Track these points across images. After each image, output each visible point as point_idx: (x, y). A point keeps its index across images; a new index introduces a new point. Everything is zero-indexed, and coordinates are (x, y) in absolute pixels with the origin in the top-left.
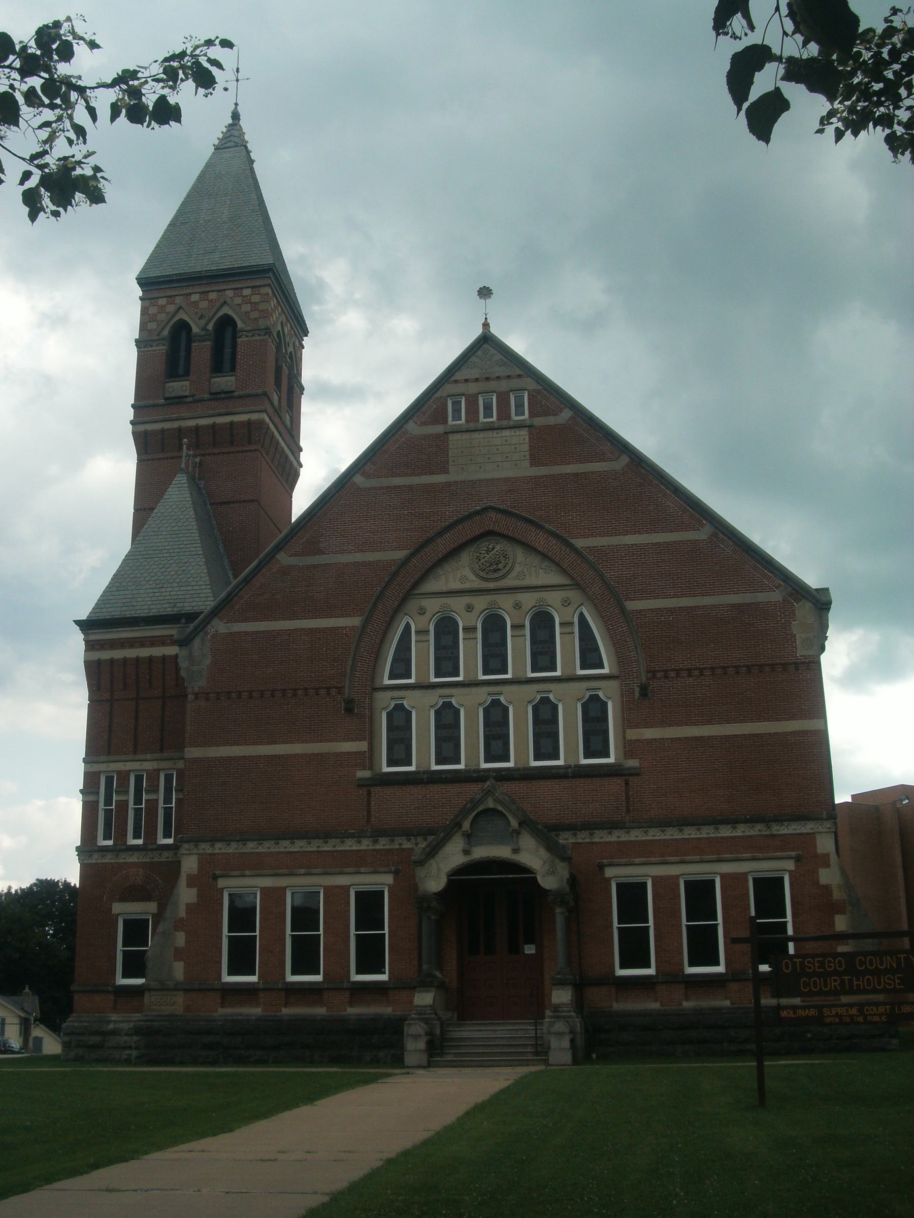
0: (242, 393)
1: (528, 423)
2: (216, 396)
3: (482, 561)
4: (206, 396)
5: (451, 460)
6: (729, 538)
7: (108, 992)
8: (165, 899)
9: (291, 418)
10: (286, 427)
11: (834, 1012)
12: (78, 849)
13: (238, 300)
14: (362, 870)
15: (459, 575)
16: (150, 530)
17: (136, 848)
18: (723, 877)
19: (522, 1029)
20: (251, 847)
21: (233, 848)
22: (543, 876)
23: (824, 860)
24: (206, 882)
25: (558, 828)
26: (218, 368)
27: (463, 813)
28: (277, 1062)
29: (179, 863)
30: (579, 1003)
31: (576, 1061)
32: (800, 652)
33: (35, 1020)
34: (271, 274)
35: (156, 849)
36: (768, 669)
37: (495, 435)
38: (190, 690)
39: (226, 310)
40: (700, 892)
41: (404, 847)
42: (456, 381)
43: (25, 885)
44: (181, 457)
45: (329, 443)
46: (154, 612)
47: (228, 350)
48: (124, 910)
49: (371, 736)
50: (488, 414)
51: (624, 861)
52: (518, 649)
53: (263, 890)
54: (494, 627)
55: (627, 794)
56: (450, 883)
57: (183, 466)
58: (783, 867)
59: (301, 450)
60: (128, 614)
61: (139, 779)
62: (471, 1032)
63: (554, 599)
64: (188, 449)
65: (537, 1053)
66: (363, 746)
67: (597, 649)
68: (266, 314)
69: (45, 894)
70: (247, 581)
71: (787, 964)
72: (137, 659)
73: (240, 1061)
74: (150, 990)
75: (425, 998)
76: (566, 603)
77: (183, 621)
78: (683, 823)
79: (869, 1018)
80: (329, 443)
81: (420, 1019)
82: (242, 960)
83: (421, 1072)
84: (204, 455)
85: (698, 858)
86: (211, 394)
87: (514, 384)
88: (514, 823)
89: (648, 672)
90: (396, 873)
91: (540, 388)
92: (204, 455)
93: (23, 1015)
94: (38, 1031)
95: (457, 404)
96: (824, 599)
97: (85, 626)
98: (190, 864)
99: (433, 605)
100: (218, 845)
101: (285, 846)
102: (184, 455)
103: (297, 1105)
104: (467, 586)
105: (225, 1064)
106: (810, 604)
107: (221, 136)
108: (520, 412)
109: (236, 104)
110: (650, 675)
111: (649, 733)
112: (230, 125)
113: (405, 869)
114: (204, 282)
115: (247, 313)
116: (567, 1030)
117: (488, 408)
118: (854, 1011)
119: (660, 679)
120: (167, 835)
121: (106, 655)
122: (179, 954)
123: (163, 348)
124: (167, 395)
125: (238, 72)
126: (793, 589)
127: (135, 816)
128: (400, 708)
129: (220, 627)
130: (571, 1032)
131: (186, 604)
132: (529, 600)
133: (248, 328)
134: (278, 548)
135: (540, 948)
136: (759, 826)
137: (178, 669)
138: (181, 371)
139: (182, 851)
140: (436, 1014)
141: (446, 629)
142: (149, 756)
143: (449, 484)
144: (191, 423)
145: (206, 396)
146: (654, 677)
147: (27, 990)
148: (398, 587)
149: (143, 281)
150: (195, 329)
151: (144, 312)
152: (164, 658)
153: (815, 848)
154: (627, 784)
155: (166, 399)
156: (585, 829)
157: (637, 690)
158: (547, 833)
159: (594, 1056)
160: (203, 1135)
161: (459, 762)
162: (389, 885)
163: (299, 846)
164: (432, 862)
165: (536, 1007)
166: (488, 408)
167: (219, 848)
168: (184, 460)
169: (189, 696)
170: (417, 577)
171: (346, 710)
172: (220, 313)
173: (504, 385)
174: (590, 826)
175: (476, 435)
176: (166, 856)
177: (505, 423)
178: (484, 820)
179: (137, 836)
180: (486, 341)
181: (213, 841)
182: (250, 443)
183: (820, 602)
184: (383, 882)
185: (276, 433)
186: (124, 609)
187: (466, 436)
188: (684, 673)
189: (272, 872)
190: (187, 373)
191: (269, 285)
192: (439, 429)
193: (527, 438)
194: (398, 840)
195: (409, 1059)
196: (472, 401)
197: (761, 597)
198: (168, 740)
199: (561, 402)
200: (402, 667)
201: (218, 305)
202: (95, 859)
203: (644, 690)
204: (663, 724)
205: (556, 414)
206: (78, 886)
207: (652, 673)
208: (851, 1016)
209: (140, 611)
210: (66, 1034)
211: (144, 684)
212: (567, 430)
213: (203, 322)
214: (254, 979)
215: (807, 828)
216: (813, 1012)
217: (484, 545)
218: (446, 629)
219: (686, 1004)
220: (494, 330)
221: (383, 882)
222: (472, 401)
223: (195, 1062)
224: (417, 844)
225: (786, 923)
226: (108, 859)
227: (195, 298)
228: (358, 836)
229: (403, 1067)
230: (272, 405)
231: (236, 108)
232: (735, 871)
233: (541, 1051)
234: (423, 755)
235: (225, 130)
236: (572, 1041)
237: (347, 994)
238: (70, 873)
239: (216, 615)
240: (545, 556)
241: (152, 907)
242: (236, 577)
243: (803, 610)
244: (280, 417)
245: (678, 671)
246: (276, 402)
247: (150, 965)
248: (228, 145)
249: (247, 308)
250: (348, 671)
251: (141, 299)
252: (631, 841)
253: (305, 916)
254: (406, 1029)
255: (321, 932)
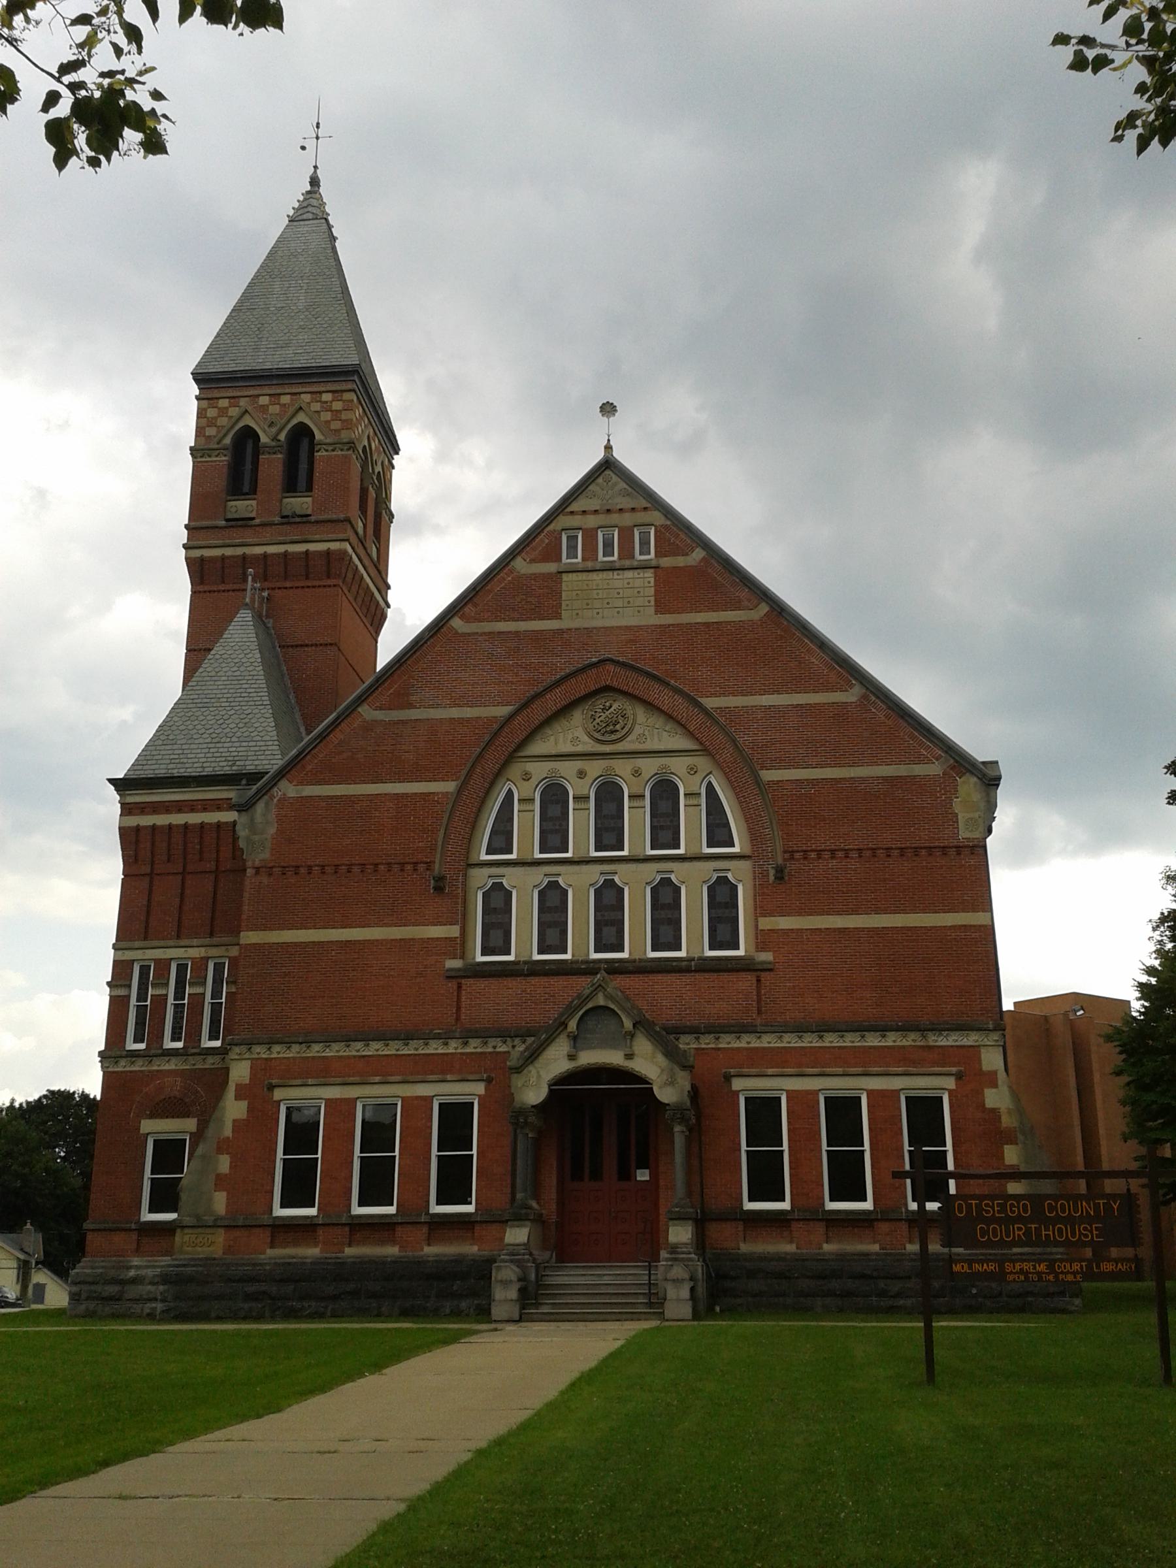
0: (321, 517)
1: (654, 563)
2: (290, 520)
3: (598, 720)
4: (277, 519)
5: (564, 604)
6: (882, 701)
7: (131, 1230)
8: (206, 1112)
9: (378, 550)
10: (372, 560)
11: (1018, 1267)
12: (101, 1054)
13: (316, 406)
14: (449, 1077)
15: (570, 737)
16: (205, 674)
17: (174, 1053)
18: (870, 1093)
19: (631, 1274)
20: (316, 1050)
21: (295, 1051)
22: (660, 1088)
23: (991, 1079)
24: (258, 1093)
25: (679, 1031)
26: (291, 486)
27: (570, 1010)
28: (336, 1316)
29: (227, 1069)
30: (701, 1242)
31: (696, 1316)
32: (964, 834)
33: (37, 1263)
34: (356, 378)
35: (199, 1054)
36: (924, 852)
37: (616, 577)
38: (249, 864)
39: (301, 418)
40: (843, 1111)
41: (498, 1050)
42: (572, 513)
43: (34, 1096)
44: (245, 590)
45: (423, 579)
46: (208, 771)
47: (303, 466)
48: (154, 1128)
49: (464, 921)
50: (608, 551)
51: (754, 1071)
52: (636, 823)
53: (329, 1102)
54: (609, 796)
55: (759, 995)
56: (551, 1091)
57: (247, 600)
58: (940, 1084)
59: (389, 587)
60: (175, 773)
61: (182, 969)
62: (573, 1276)
63: (678, 766)
64: (254, 580)
65: (650, 1305)
66: (454, 931)
67: (727, 825)
68: (348, 425)
69: (59, 1104)
70: (322, 737)
71: (960, 1206)
72: (186, 826)
73: (292, 1314)
74: (183, 1227)
75: (517, 1235)
76: (693, 771)
77: (244, 782)
78: (822, 1029)
79: (1061, 1276)
80: (423, 579)
81: (511, 1261)
82: (298, 1188)
83: (510, 1327)
84: (273, 589)
85: (840, 1070)
86: (283, 517)
87: (641, 517)
88: (628, 1024)
89: (785, 852)
90: (489, 1081)
91: (669, 523)
92: (273, 589)
93: (22, 1257)
94: (40, 1277)
95: (572, 539)
96: (991, 773)
97: (119, 784)
98: (240, 1072)
99: (540, 770)
100: (276, 1048)
101: (357, 1049)
102: (249, 587)
103: (361, 1375)
104: (580, 749)
105: (273, 1319)
106: (975, 779)
107: (297, 205)
108: (645, 550)
109: (316, 167)
110: (787, 856)
111: (785, 923)
112: (308, 192)
113: (499, 1075)
114: (275, 382)
115: (328, 422)
116: (687, 1276)
117: (608, 545)
118: (1042, 1267)
119: (798, 860)
120: (213, 1036)
121: (147, 821)
122: (221, 1182)
123: (224, 459)
124: (229, 516)
125: (318, 127)
126: (957, 762)
127: (175, 1013)
128: (498, 887)
129: (288, 789)
130: (691, 1279)
131: (247, 763)
132: (650, 767)
133: (328, 441)
134: (361, 700)
135: (654, 1176)
136: (913, 1036)
137: (235, 839)
138: (246, 489)
139: (232, 1055)
140: (531, 1254)
141: (554, 798)
142: (195, 942)
143: (561, 632)
144: (258, 550)
145: (277, 519)
146: (792, 858)
147: (28, 1226)
148: (495, 751)
149: (200, 377)
150: (264, 439)
151: (201, 414)
152: (219, 825)
153: (980, 1064)
154: (758, 981)
155: (227, 520)
156: (710, 1033)
157: (772, 872)
158: (666, 1037)
159: (718, 1309)
160: (243, 1418)
161: (565, 952)
162: (479, 1096)
163: (375, 1048)
164: (531, 1068)
165: (648, 1246)
166: (608, 545)
167: (278, 1052)
168: (249, 593)
169: (248, 870)
170: (521, 737)
171: (435, 888)
172: (295, 421)
173: (627, 519)
174: (716, 1030)
175: (594, 576)
176: (211, 1062)
177: (627, 563)
178: (593, 1020)
179: (175, 1038)
180: (608, 465)
181: (271, 1043)
182: (329, 577)
183: (988, 778)
184: (472, 1091)
185: (360, 567)
186: (171, 766)
187: (583, 576)
188: (827, 855)
189: (339, 1080)
190: (254, 491)
191: (354, 391)
192: (551, 567)
193: (652, 580)
194: (492, 1042)
195: (497, 1311)
196: (590, 536)
197: (919, 770)
198: (220, 922)
199: (693, 541)
200: (502, 839)
201: (291, 410)
202: (122, 1066)
203: (780, 873)
204: (801, 912)
205: (687, 554)
206: (98, 1098)
207: (790, 854)
208: (1039, 1274)
209: (193, 769)
210: (75, 1283)
211: (184, 854)
212: (701, 573)
213: (274, 430)
214: (312, 1212)
215: (971, 1039)
216: (992, 1267)
217: (600, 702)
218: (554, 798)
219: (827, 1247)
220: (617, 454)
221: (472, 1091)
222: (590, 536)
223: (235, 1317)
224: (514, 1047)
225: (945, 1152)
226: (138, 1066)
227: (264, 400)
228: (445, 1038)
229: (490, 1322)
230: (357, 534)
231: (315, 172)
232: (885, 1087)
233: (655, 1302)
234: (525, 944)
235: (301, 198)
236: (692, 1289)
237: (425, 1229)
238: (89, 1081)
239: (283, 776)
240: (670, 717)
241: (191, 1124)
242: (309, 732)
243: (968, 786)
244: (365, 548)
245: (819, 852)
246: (360, 530)
247: (184, 1196)
248: (305, 217)
249: (326, 416)
250: (440, 843)
251: (197, 398)
252: (764, 1048)
253: (378, 1134)
254: (494, 1274)
255: (397, 1153)
